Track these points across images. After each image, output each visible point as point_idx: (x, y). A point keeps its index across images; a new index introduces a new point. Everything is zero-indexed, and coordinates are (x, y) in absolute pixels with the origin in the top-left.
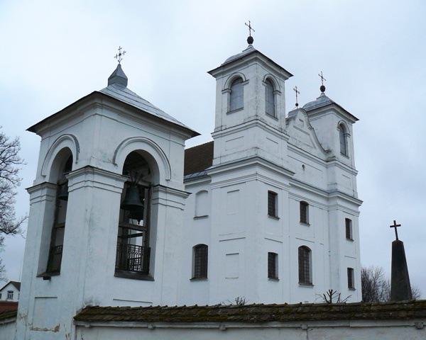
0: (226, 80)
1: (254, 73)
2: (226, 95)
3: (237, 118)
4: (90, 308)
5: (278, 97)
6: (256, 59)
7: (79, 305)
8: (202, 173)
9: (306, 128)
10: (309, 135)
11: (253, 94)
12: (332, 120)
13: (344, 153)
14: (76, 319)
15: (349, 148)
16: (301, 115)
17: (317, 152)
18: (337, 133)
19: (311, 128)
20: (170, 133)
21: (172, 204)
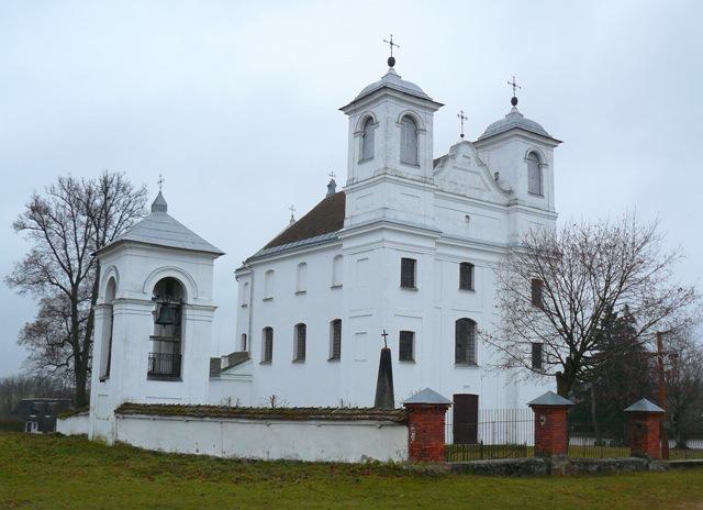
0: (359, 117)
1: (388, 112)
2: (358, 140)
3: (366, 171)
4: (126, 404)
5: (421, 137)
6: (386, 95)
7: (119, 402)
8: (333, 235)
9: (474, 166)
10: (479, 174)
11: (389, 138)
12: (519, 148)
13: (537, 191)
14: (115, 412)
15: (545, 184)
16: (466, 150)
17: (493, 195)
18: (523, 168)
19: (482, 165)
20: (198, 257)
21: (200, 318)
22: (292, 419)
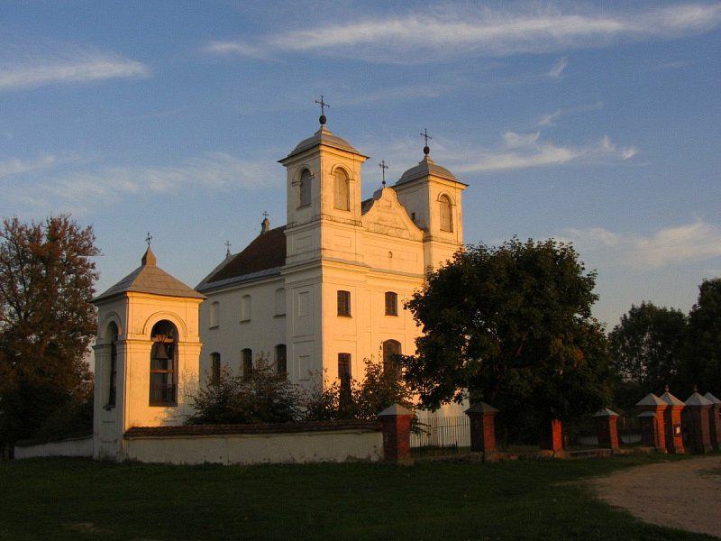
0: (296, 169)
22: (289, 432)
